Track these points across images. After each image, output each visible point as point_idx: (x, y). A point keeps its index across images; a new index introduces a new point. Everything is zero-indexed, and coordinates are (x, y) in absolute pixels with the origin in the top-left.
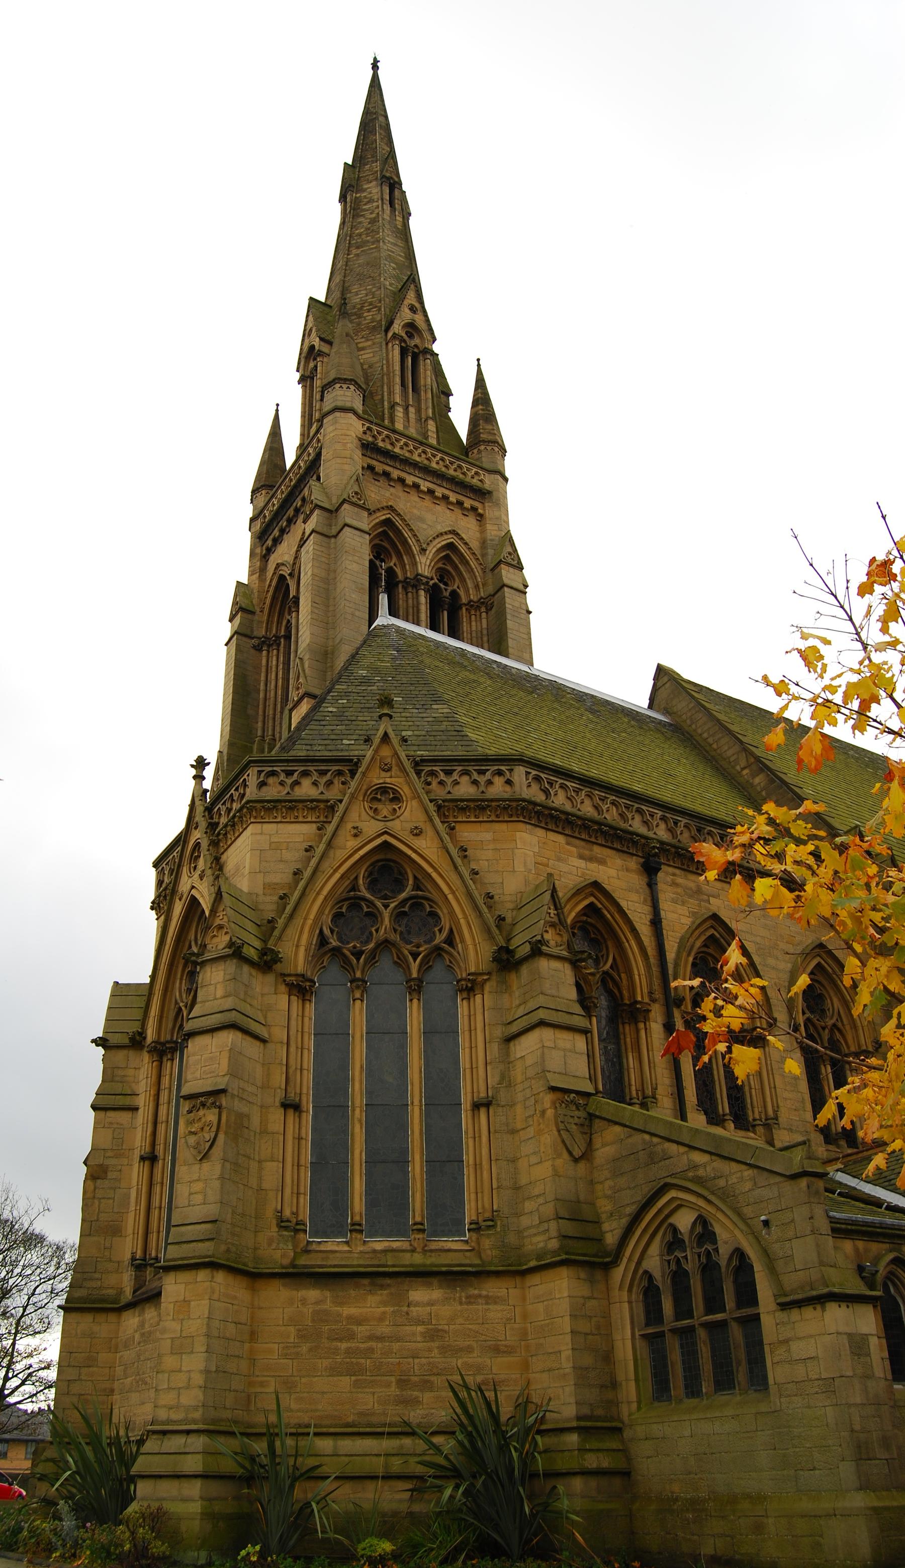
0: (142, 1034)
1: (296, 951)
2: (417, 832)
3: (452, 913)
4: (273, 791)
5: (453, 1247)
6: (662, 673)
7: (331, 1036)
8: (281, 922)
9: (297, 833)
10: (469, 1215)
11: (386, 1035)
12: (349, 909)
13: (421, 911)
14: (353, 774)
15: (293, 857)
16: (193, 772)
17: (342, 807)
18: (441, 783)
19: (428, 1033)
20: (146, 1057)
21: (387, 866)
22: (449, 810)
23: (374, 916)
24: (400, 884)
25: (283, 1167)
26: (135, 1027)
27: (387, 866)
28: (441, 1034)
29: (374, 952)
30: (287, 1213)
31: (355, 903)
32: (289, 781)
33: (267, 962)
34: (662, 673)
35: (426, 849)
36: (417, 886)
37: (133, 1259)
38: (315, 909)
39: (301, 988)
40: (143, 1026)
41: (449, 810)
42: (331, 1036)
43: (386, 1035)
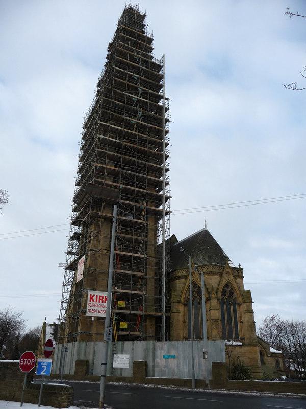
9: (183, 280)
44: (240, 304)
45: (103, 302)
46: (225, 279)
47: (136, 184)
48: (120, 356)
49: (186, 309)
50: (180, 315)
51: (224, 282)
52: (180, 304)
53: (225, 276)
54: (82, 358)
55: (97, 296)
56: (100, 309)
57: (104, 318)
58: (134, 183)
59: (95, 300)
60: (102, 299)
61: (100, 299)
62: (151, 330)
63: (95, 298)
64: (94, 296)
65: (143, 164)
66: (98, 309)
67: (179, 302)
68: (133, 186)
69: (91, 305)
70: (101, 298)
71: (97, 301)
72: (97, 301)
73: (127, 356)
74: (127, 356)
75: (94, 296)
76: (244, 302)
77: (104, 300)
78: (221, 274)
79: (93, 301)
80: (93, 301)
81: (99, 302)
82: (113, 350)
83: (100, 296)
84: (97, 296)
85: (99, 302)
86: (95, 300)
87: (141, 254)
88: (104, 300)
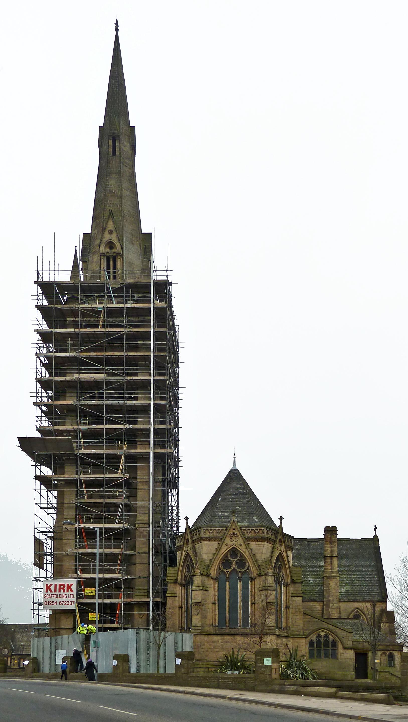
0: (177, 580)
1: (213, 572)
2: (241, 545)
3: (248, 563)
4: (208, 534)
5: (246, 629)
6: (19, 438)
7: (222, 590)
8: (211, 566)
9: (215, 544)
10: (250, 623)
11: (234, 589)
12: (226, 562)
13: (242, 562)
14: (226, 530)
15: (213, 551)
16: (185, 521)
17: (224, 538)
18: (247, 532)
19: (243, 588)
20: (178, 585)
21: (234, 552)
22: (248, 539)
23: (231, 563)
24: (236, 556)
25: (212, 613)
26: (175, 578)
27: (234, 552)
28: (245, 588)
29: (231, 571)
30: (214, 624)
31: (228, 560)
32: (211, 532)
33: (208, 575)
34: (19, 438)
35: (243, 550)
36: (241, 556)
37: (179, 627)
38: (218, 561)
39: (215, 579)
40: (177, 577)
41: (248, 539)
42: (222, 590)
43: (234, 589)
44: (252, 579)
45: (64, 591)
46: (227, 545)
47: (106, 418)
48: (60, 651)
49: (184, 591)
50: (177, 599)
51: (225, 549)
52: (172, 581)
53: (227, 541)
54: (180, 650)
55: (56, 585)
56: (61, 600)
57: (74, 611)
58: (102, 418)
59: (53, 590)
60: (63, 589)
61: (60, 589)
62: (140, 620)
63: (52, 588)
64: (51, 585)
65: (118, 381)
66: (58, 600)
67: (175, 582)
68: (101, 423)
69: (48, 596)
70: (62, 587)
71: (55, 591)
72: (55, 591)
73: (65, 651)
74: (65, 651)
75: (51, 585)
76: (260, 575)
77: (66, 588)
78: (220, 539)
79: (51, 591)
80: (51, 591)
81: (60, 591)
82: (56, 646)
83: (60, 585)
84: (56, 585)
85: (60, 591)
86: (53, 590)
87: (119, 523)
88: (66, 588)
